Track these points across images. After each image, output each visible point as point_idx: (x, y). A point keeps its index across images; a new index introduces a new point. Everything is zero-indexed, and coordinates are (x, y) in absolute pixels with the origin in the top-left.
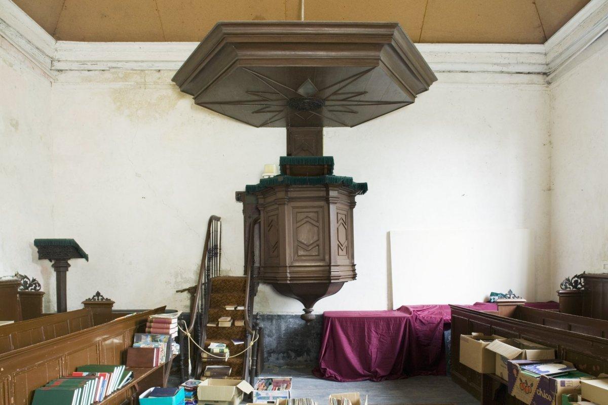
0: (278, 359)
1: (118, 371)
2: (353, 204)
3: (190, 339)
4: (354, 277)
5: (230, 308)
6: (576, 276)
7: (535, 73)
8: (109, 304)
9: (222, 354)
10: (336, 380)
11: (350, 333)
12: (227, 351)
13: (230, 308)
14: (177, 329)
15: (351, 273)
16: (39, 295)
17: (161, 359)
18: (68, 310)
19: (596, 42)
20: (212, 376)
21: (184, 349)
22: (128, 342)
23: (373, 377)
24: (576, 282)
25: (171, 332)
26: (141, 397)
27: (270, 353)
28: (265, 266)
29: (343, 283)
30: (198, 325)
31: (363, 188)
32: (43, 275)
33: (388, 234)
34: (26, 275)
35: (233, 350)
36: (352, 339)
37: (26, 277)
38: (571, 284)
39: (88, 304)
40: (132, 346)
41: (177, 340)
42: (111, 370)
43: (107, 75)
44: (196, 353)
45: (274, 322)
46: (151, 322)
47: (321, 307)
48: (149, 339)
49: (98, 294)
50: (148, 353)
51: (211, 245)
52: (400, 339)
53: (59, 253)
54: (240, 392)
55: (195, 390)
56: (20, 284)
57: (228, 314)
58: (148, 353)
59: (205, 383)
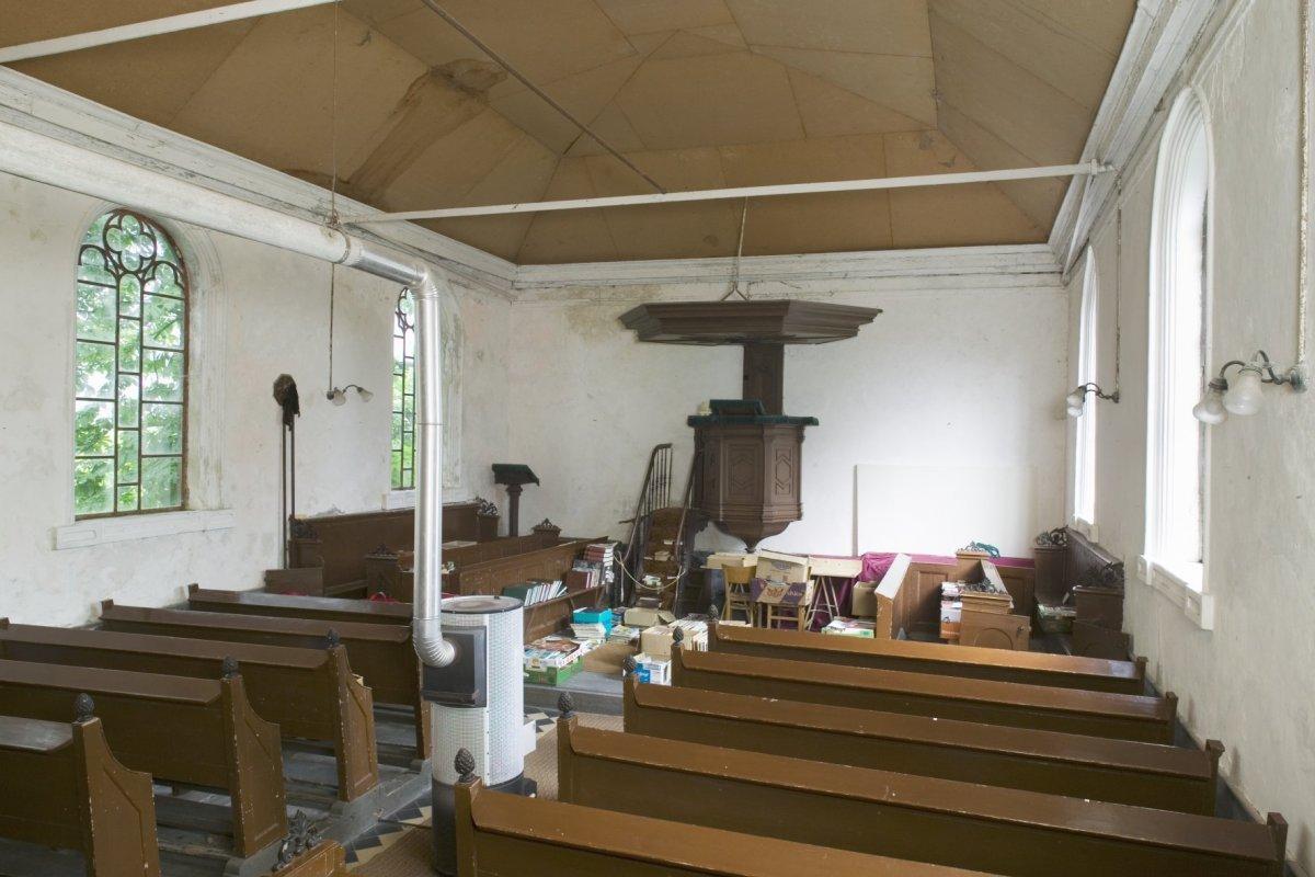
1: (557, 585)
2: (800, 438)
4: (799, 517)
5: (668, 543)
6: (1056, 530)
7: (1047, 273)
8: (556, 531)
9: (655, 585)
12: (659, 584)
13: (668, 543)
14: (612, 559)
15: (796, 513)
16: (495, 519)
18: (520, 535)
19: (1203, 200)
20: (642, 607)
24: (1056, 537)
25: (605, 560)
29: (788, 523)
30: (633, 557)
31: (812, 421)
32: (497, 498)
33: (856, 467)
37: (484, 501)
38: (1050, 539)
39: (538, 529)
42: (551, 583)
43: (564, 292)
44: (630, 587)
48: (586, 564)
49: (547, 521)
51: (654, 476)
53: (513, 477)
55: (623, 615)
56: (479, 508)
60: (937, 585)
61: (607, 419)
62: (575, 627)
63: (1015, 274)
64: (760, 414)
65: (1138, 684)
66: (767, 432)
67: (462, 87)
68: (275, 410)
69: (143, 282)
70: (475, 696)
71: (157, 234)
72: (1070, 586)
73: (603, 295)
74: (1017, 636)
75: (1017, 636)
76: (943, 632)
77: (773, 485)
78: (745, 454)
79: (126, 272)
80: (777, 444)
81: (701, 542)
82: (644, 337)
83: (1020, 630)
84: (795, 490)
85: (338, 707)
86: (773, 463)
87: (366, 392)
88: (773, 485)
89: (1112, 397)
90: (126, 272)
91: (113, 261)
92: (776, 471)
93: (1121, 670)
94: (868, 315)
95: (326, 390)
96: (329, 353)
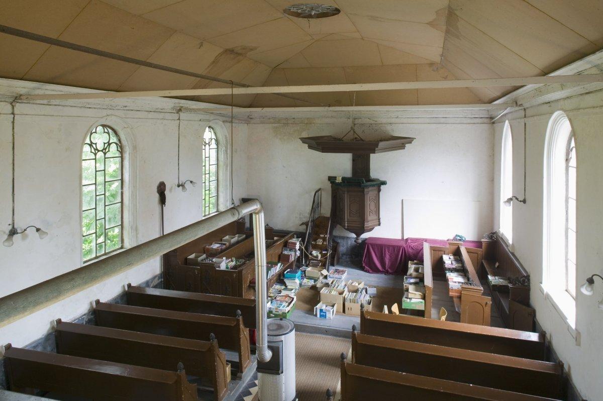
0: (346, 258)
1: (279, 264)
2: (379, 190)
3: (305, 252)
4: (379, 225)
5: (322, 236)
9: (317, 257)
10: (369, 272)
11: (376, 250)
17: (292, 259)
21: (301, 253)
22: (280, 251)
23: (386, 272)
24: (492, 236)
26: (285, 273)
27: (343, 255)
28: (337, 216)
31: (384, 183)
33: (402, 200)
34: (504, 233)
35: (323, 256)
36: (377, 255)
40: (282, 253)
41: (299, 250)
44: (306, 257)
45: (345, 240)
46: (289, 243)
47: (365, 236)
50: (288, 257)
52: (400, 256)
54: (322, 275)
57: (321, 238)
58: (288, 257)
59: (309, 269)
60: (440, 255)
61: (295, 179)
62: (286, 281)
63: (471, 118)
64: (363, 183)
65: (543, 349)
66: (366, 190)
67: (237, 53)
68: (156, 197)
69: (105, 154)
70: (280, 372)
71: (110, 131)
72: (501, 270)
73: (289, 122)
74: (486, 306)
75: (486, 306)
76: (450, 293)
77: (368, 213)
78: (354, 194)
79: (99, 151)
80: (370, 194)
81: (336, 233)
82: (310, 147)
83: (487, 303)
84: (378, 212)
85: (215, 366)
86: (369, 203)
87: (194, 183)
88: (368, 213)
89: (523, 201)
90: (99, 151)
91: (94, 148)
92: (369, 205)
93: (534, 337)
94: (409, 140)
95: (177, 183)
96: (178, 168)
